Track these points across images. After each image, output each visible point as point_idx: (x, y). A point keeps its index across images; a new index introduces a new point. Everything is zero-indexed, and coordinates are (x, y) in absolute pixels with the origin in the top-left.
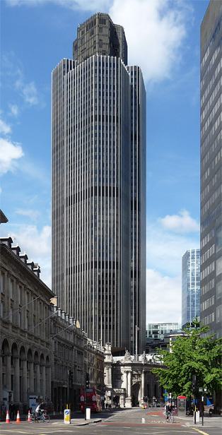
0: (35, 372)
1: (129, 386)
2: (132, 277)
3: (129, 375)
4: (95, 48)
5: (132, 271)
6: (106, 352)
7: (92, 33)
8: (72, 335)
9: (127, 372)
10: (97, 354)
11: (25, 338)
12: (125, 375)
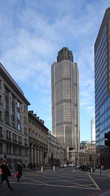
0: (40, 153)
3: (75, 156)
7: (63, 53)
10: (64, 149)
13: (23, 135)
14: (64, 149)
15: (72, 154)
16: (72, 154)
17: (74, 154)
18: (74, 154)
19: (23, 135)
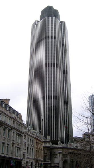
1: (61, 162)
3: (61, 155)
6: (48, 140)
9: (60, 153)
10: (35, 138)
12: (58, 155)
14: (35, 138)
15: (57, 151)
16: (57, 151)
17: (60, 151)
18: (60, 151)
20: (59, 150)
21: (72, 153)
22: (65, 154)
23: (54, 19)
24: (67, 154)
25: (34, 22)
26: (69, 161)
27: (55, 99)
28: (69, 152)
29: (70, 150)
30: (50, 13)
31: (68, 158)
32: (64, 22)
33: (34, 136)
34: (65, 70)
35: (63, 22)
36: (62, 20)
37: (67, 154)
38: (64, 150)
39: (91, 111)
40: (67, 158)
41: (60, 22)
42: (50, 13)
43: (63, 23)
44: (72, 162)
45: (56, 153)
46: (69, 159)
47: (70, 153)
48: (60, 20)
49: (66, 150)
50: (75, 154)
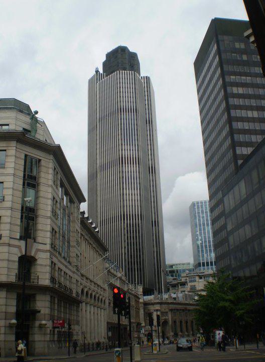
2: (150, 173)
4: (118, 66)
5: (152, 221)
8: (118, 281)
9: (157, 310)
11: (92, 287)
13: (74, 272)
15: (152, 308)
16: (152, 308)
19: (74, 272)
20: (155, 306)
21: (174, 309)
22: (164, 311)
23: (132, 75)
24: (167, 312)
25: (94, 76)
26: (170, 321)
27: (136, 164)
28: (170, 308)
29: (170, 306)
30: (121, 61)
31: (169, 317)
32: (149, 77)
33: (133, 292)
34: (155, 221)
35: (146, 77)
36: (143, 73)
37: (167, 312)
38: (163, 306)
39: (149, 302)
40: (167, 318)
41: (142, 77)
42: (121, 61)
43: (148, 79)
44: (175, 322)
45: (152, 311)
46: (170, 319)
47: (171, 310)
48: (140, 75)
49: (166, 306)
50: (177, 310)
